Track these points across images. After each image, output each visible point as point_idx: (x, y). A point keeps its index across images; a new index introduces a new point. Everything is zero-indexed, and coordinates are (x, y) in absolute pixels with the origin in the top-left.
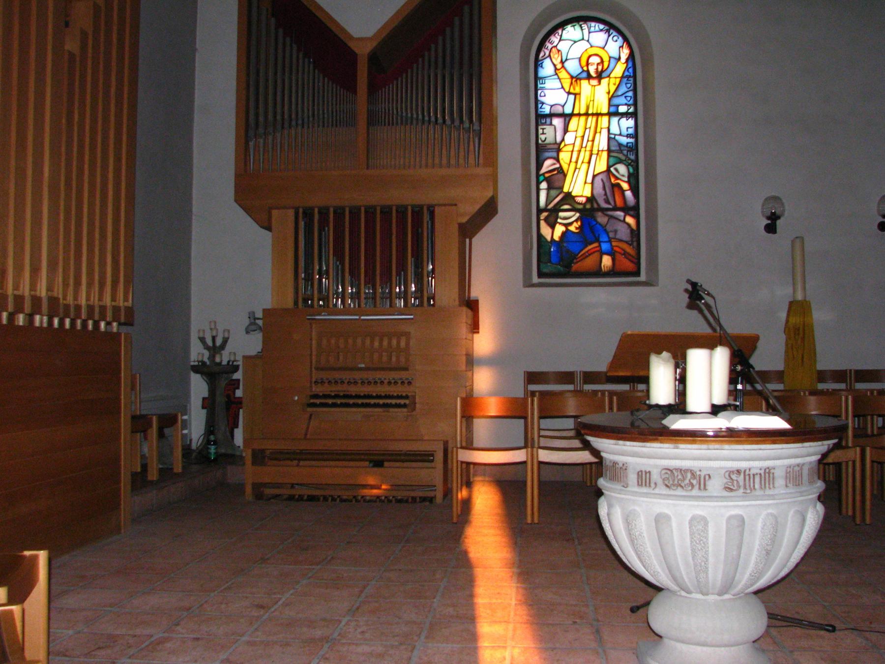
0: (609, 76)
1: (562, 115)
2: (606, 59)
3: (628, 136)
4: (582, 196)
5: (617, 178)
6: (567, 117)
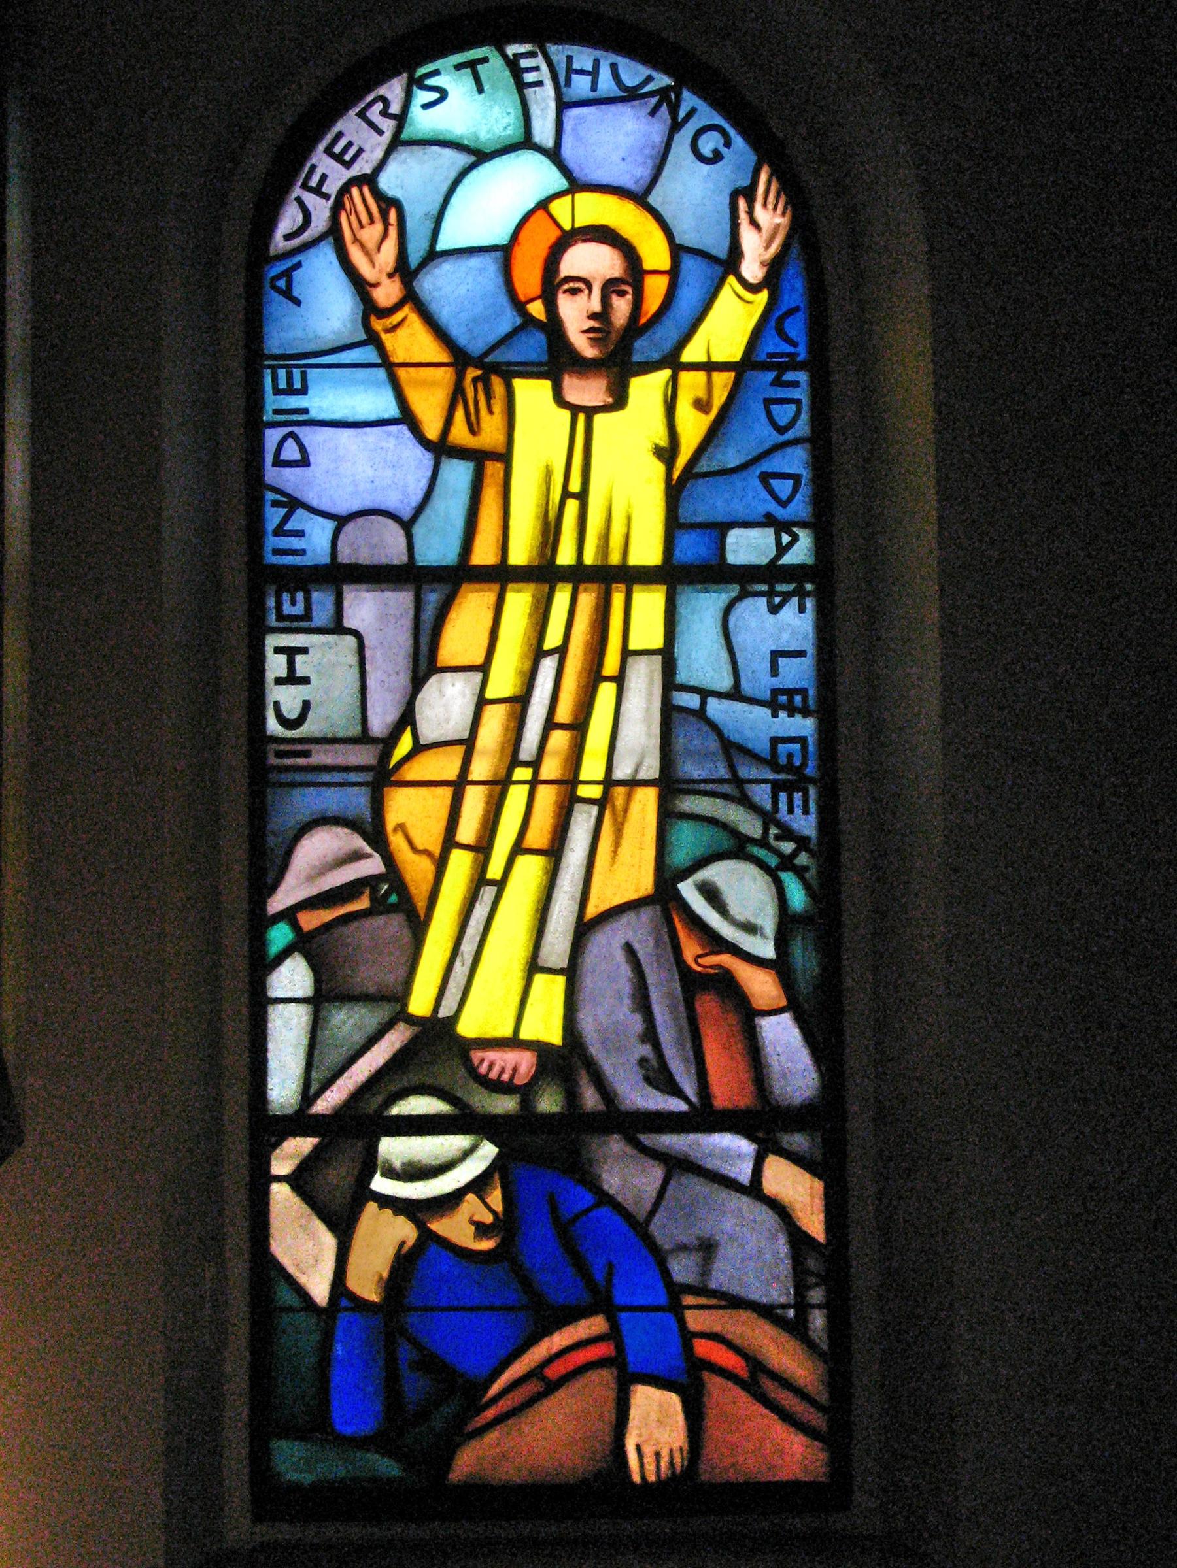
0: (672, 361)
1: (406, 575)
2: (655, 253)
3: (780, 701)
4: (514, 1042)
5: (717, 943)
6: (434, 587)
